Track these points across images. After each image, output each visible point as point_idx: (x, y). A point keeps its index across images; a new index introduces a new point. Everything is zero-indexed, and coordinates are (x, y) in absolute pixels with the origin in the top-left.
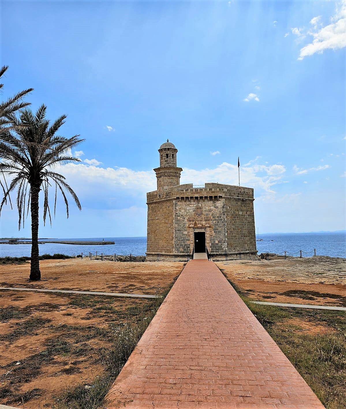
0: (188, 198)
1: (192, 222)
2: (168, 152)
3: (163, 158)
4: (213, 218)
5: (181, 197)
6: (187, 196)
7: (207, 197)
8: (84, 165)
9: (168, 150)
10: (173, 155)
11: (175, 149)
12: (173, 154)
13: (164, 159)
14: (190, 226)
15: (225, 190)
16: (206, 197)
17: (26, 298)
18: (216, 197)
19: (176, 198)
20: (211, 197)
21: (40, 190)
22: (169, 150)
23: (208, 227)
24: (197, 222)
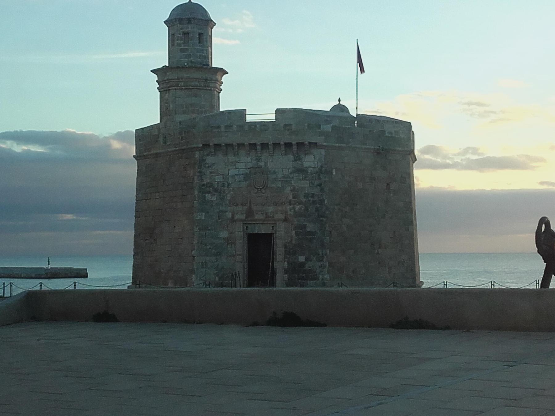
0: (231, 145)
1: (240, 208)
2: (189, 28)
3: (176, 42)
4: (293, 198)
5: (215, 145)
6: (228, 141)
7: (255, 145)
8: (178, 66)
9: (188, 23)
10: (200, 34)
11: (205, 20)
12: (200, 31)
13: (179, 45)
14: (236, 217)
15: (328, 128)
16: (276, 145)
17: (237, 271)
18: (300, 145)
19: (201, 145)
20: (288, 145)
21: (341, 103)
22: (191, 24)
23: (279, 220)
24: (254, 208)
